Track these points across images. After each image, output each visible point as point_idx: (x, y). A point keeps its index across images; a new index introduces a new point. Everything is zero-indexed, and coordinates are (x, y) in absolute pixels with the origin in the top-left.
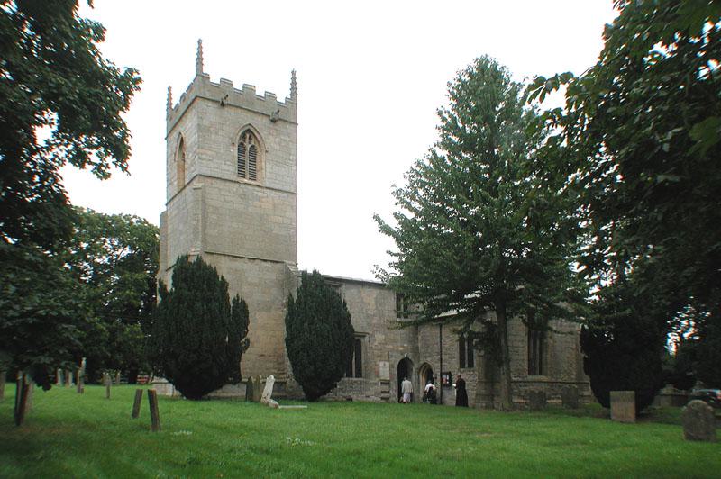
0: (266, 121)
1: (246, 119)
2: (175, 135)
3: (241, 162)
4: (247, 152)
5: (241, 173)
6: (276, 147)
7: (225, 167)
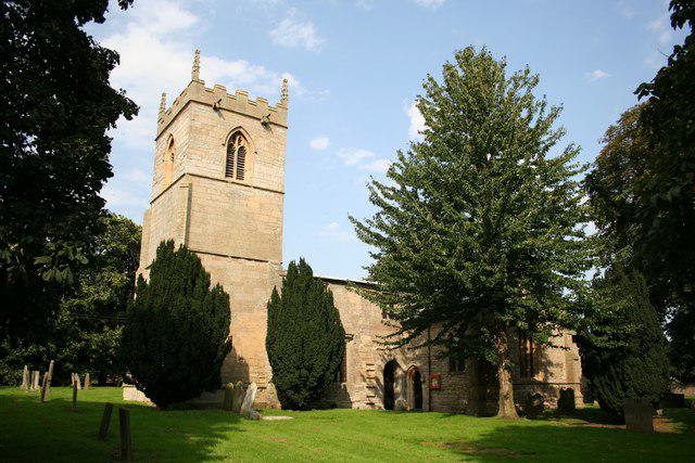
0: (258, 124)
1: (235, 121)
2: (166, 136)
3: (229, 162)
4: (236, 153)
5: (228, 173)
6: (266, 148)
7: (214, 167)
